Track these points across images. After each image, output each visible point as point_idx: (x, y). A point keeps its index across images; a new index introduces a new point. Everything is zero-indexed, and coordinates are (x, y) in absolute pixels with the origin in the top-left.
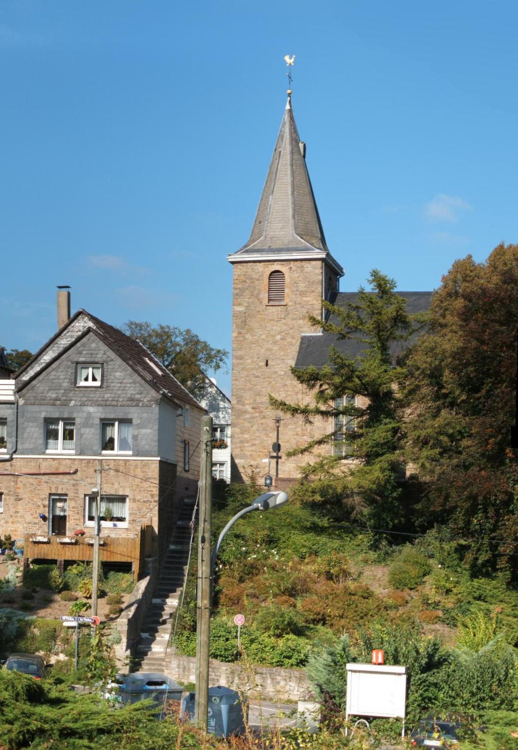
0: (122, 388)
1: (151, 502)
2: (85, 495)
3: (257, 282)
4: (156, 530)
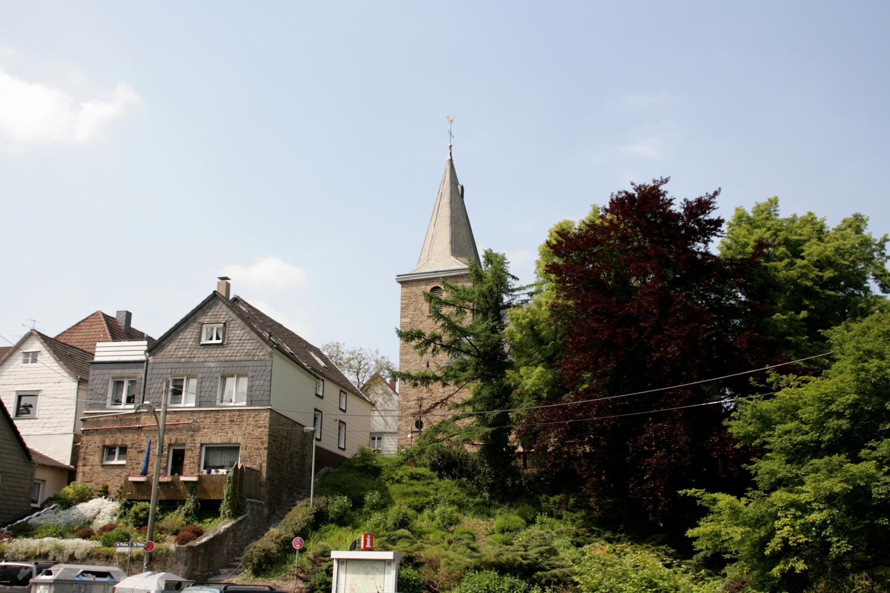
0: (240, 345)
2: (202, 445)
4: (264, 474)
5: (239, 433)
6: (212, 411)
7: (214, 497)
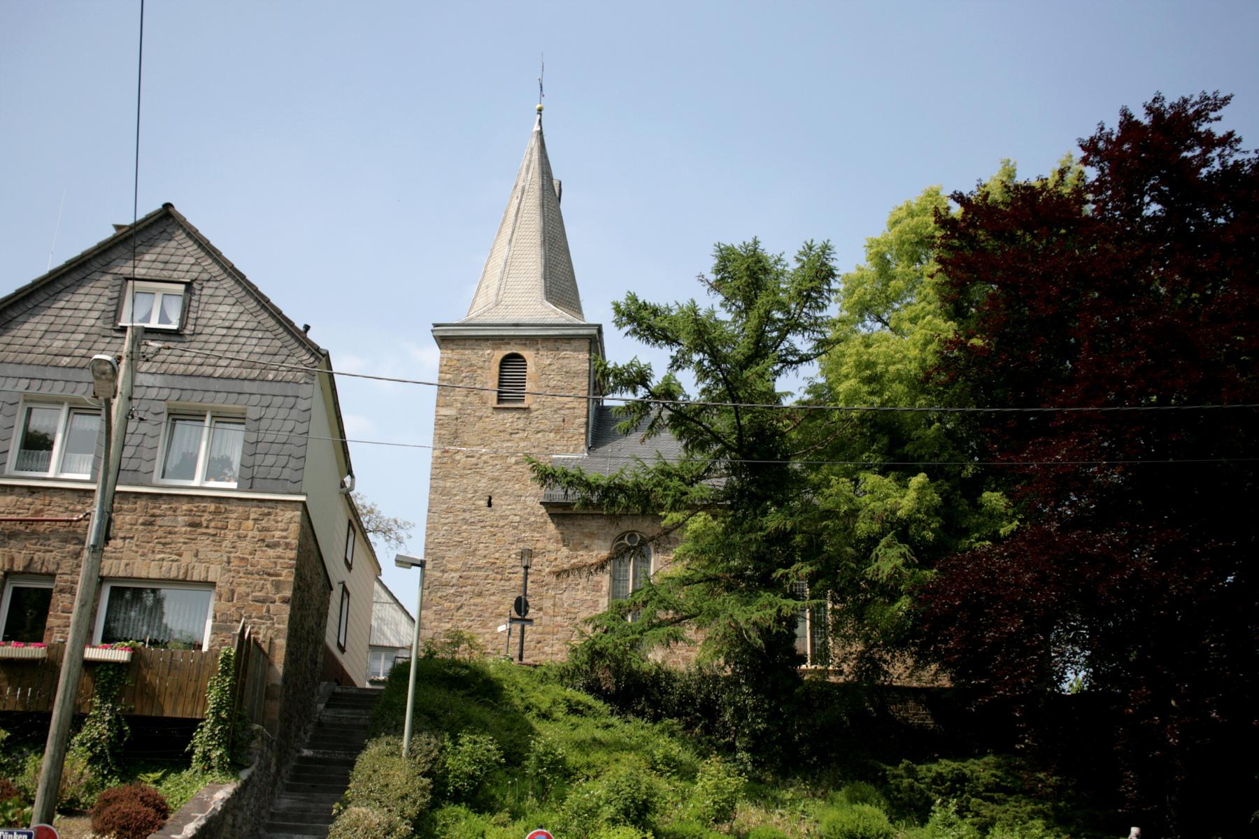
0: (229, 340)
3: (479, 371)
5: (212, 555)
6: (138, 495)
7: (174, 709)
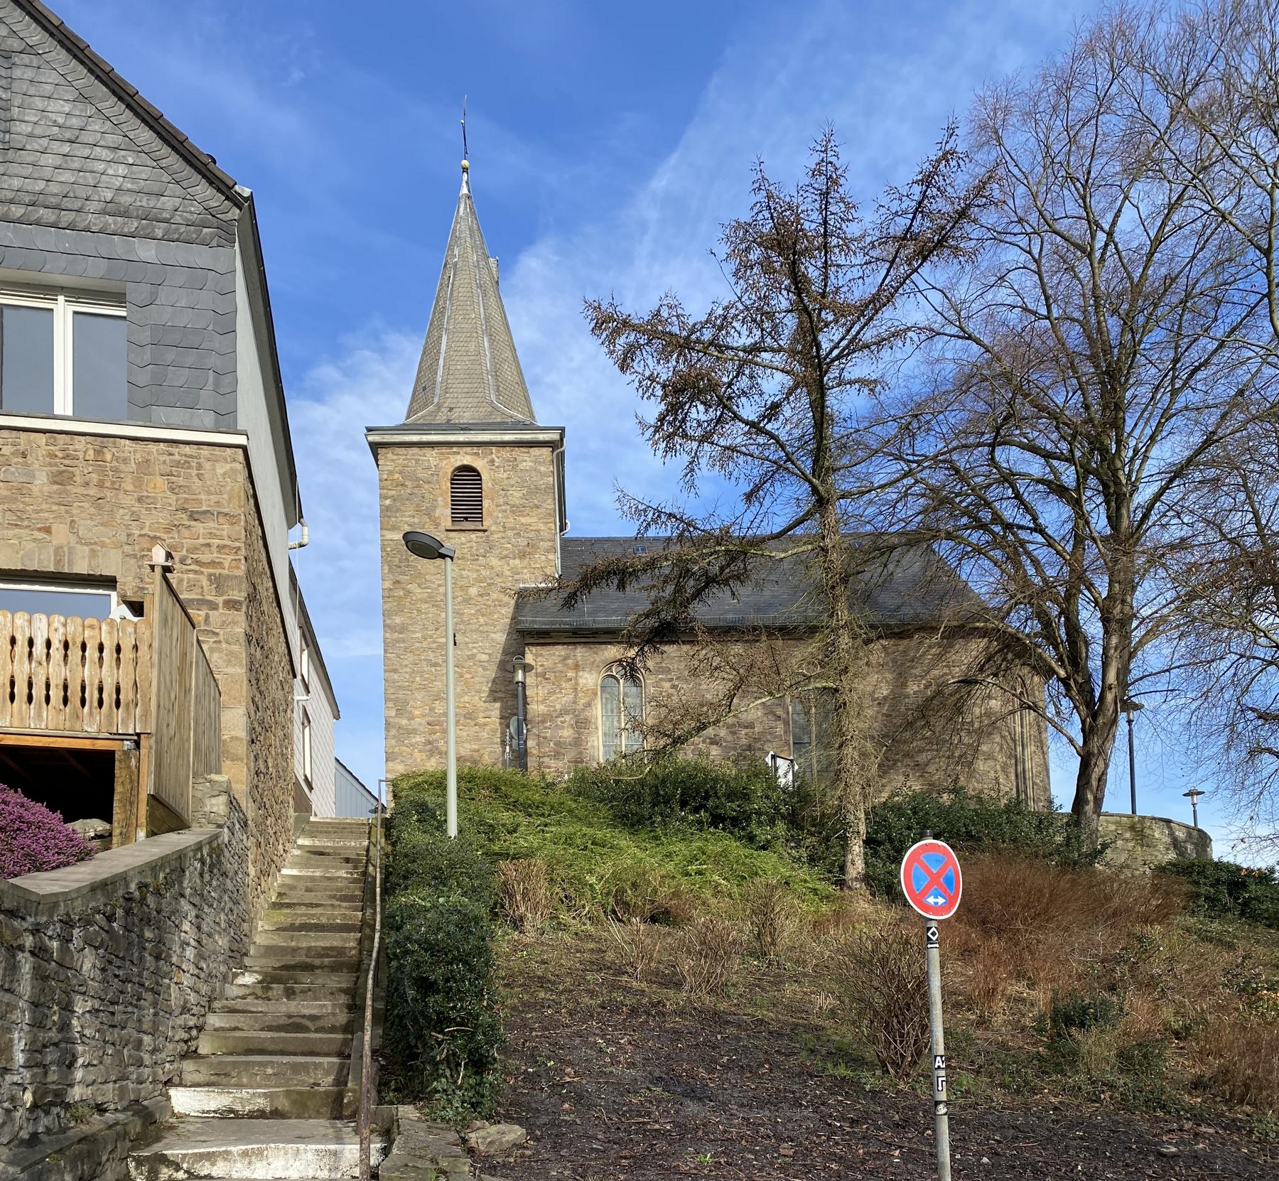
1: (213, 606)
